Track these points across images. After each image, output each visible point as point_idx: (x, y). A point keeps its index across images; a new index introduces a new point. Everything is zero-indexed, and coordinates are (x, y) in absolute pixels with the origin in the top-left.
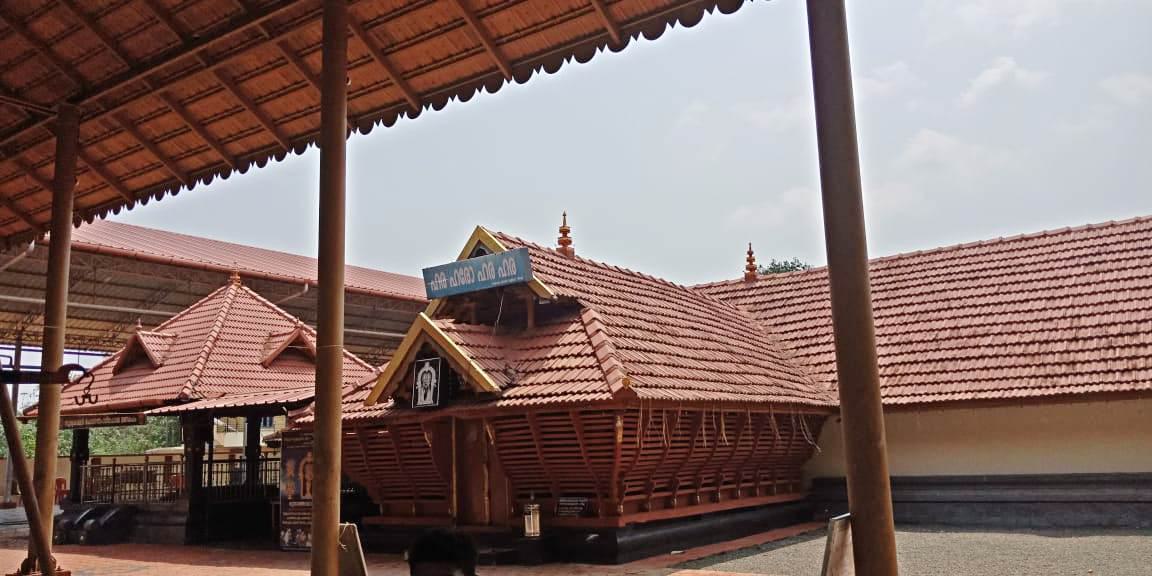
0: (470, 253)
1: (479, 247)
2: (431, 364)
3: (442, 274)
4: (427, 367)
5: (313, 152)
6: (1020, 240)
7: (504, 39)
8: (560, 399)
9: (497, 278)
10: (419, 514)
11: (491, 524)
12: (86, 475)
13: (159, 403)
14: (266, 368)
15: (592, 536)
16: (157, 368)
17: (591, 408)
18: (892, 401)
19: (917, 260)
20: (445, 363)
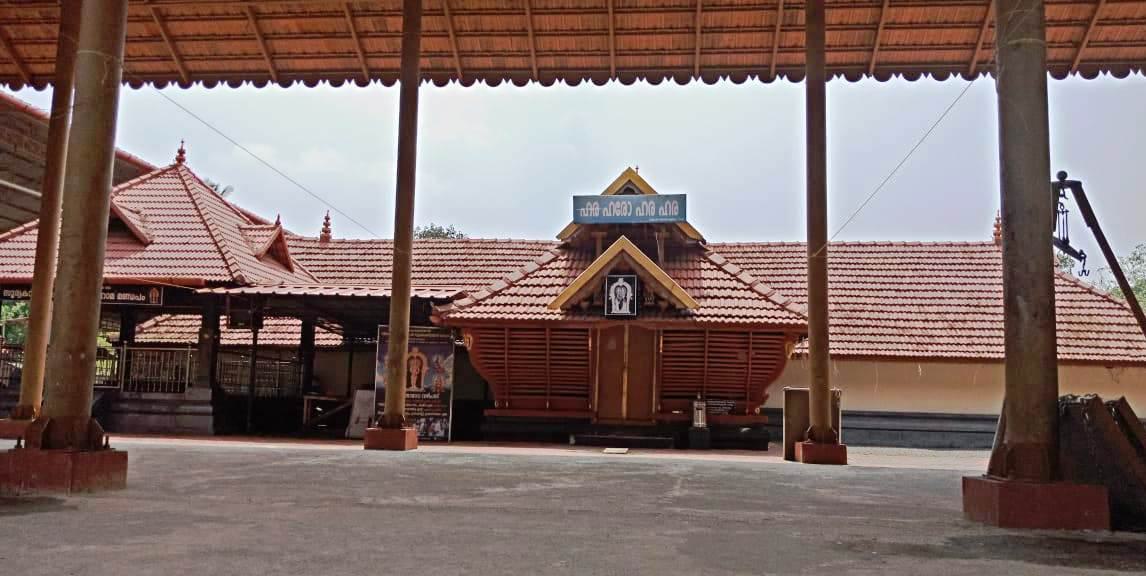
0: (617, 189)
1: (630, 185)
2: (625, 280)
3: (596, 203)
4: (621, 282)
5: (49, 90)
6: (842, 245)
8: (756, 321)
9: (657, 215)
10: (552, 409)
11: (628, 419)
13: (203, 283)
14: (259, 260)
15: (745, 429)
16: (146, 245)
17: (784, 330)
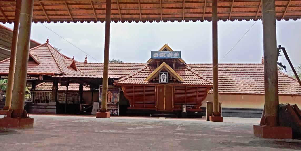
0: (162, 50)
1: (166, 49)
2: (165, 73)
4: (163, 74)
5: (13, 24)
6: (222, 64)
7: (122, 9)
8: (199, 84)
9: (173, 57)
11: (165, 110)
12: (173, 92)
13: (53, 74)
14: (68, 68)
16: (39, 64)
18: (220, 92)
19: (97, 64)
20: (169, 74)
